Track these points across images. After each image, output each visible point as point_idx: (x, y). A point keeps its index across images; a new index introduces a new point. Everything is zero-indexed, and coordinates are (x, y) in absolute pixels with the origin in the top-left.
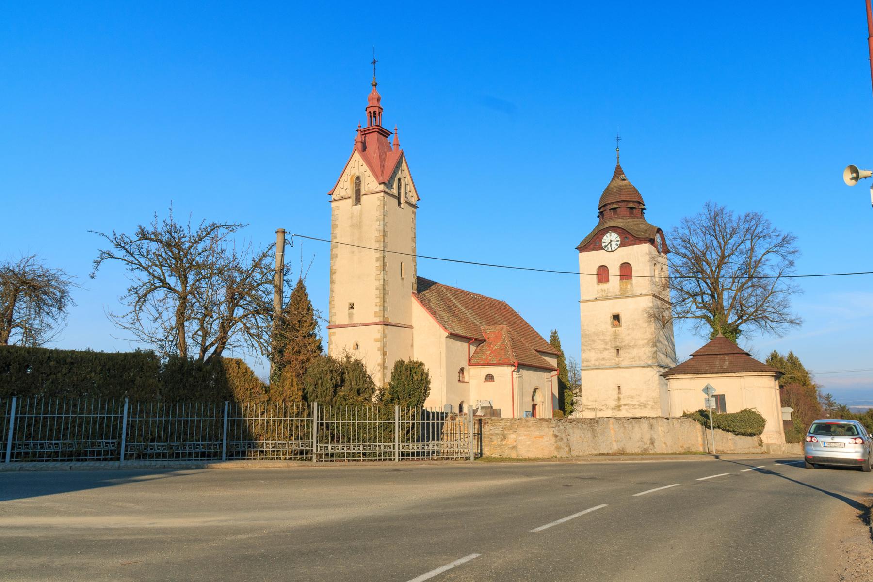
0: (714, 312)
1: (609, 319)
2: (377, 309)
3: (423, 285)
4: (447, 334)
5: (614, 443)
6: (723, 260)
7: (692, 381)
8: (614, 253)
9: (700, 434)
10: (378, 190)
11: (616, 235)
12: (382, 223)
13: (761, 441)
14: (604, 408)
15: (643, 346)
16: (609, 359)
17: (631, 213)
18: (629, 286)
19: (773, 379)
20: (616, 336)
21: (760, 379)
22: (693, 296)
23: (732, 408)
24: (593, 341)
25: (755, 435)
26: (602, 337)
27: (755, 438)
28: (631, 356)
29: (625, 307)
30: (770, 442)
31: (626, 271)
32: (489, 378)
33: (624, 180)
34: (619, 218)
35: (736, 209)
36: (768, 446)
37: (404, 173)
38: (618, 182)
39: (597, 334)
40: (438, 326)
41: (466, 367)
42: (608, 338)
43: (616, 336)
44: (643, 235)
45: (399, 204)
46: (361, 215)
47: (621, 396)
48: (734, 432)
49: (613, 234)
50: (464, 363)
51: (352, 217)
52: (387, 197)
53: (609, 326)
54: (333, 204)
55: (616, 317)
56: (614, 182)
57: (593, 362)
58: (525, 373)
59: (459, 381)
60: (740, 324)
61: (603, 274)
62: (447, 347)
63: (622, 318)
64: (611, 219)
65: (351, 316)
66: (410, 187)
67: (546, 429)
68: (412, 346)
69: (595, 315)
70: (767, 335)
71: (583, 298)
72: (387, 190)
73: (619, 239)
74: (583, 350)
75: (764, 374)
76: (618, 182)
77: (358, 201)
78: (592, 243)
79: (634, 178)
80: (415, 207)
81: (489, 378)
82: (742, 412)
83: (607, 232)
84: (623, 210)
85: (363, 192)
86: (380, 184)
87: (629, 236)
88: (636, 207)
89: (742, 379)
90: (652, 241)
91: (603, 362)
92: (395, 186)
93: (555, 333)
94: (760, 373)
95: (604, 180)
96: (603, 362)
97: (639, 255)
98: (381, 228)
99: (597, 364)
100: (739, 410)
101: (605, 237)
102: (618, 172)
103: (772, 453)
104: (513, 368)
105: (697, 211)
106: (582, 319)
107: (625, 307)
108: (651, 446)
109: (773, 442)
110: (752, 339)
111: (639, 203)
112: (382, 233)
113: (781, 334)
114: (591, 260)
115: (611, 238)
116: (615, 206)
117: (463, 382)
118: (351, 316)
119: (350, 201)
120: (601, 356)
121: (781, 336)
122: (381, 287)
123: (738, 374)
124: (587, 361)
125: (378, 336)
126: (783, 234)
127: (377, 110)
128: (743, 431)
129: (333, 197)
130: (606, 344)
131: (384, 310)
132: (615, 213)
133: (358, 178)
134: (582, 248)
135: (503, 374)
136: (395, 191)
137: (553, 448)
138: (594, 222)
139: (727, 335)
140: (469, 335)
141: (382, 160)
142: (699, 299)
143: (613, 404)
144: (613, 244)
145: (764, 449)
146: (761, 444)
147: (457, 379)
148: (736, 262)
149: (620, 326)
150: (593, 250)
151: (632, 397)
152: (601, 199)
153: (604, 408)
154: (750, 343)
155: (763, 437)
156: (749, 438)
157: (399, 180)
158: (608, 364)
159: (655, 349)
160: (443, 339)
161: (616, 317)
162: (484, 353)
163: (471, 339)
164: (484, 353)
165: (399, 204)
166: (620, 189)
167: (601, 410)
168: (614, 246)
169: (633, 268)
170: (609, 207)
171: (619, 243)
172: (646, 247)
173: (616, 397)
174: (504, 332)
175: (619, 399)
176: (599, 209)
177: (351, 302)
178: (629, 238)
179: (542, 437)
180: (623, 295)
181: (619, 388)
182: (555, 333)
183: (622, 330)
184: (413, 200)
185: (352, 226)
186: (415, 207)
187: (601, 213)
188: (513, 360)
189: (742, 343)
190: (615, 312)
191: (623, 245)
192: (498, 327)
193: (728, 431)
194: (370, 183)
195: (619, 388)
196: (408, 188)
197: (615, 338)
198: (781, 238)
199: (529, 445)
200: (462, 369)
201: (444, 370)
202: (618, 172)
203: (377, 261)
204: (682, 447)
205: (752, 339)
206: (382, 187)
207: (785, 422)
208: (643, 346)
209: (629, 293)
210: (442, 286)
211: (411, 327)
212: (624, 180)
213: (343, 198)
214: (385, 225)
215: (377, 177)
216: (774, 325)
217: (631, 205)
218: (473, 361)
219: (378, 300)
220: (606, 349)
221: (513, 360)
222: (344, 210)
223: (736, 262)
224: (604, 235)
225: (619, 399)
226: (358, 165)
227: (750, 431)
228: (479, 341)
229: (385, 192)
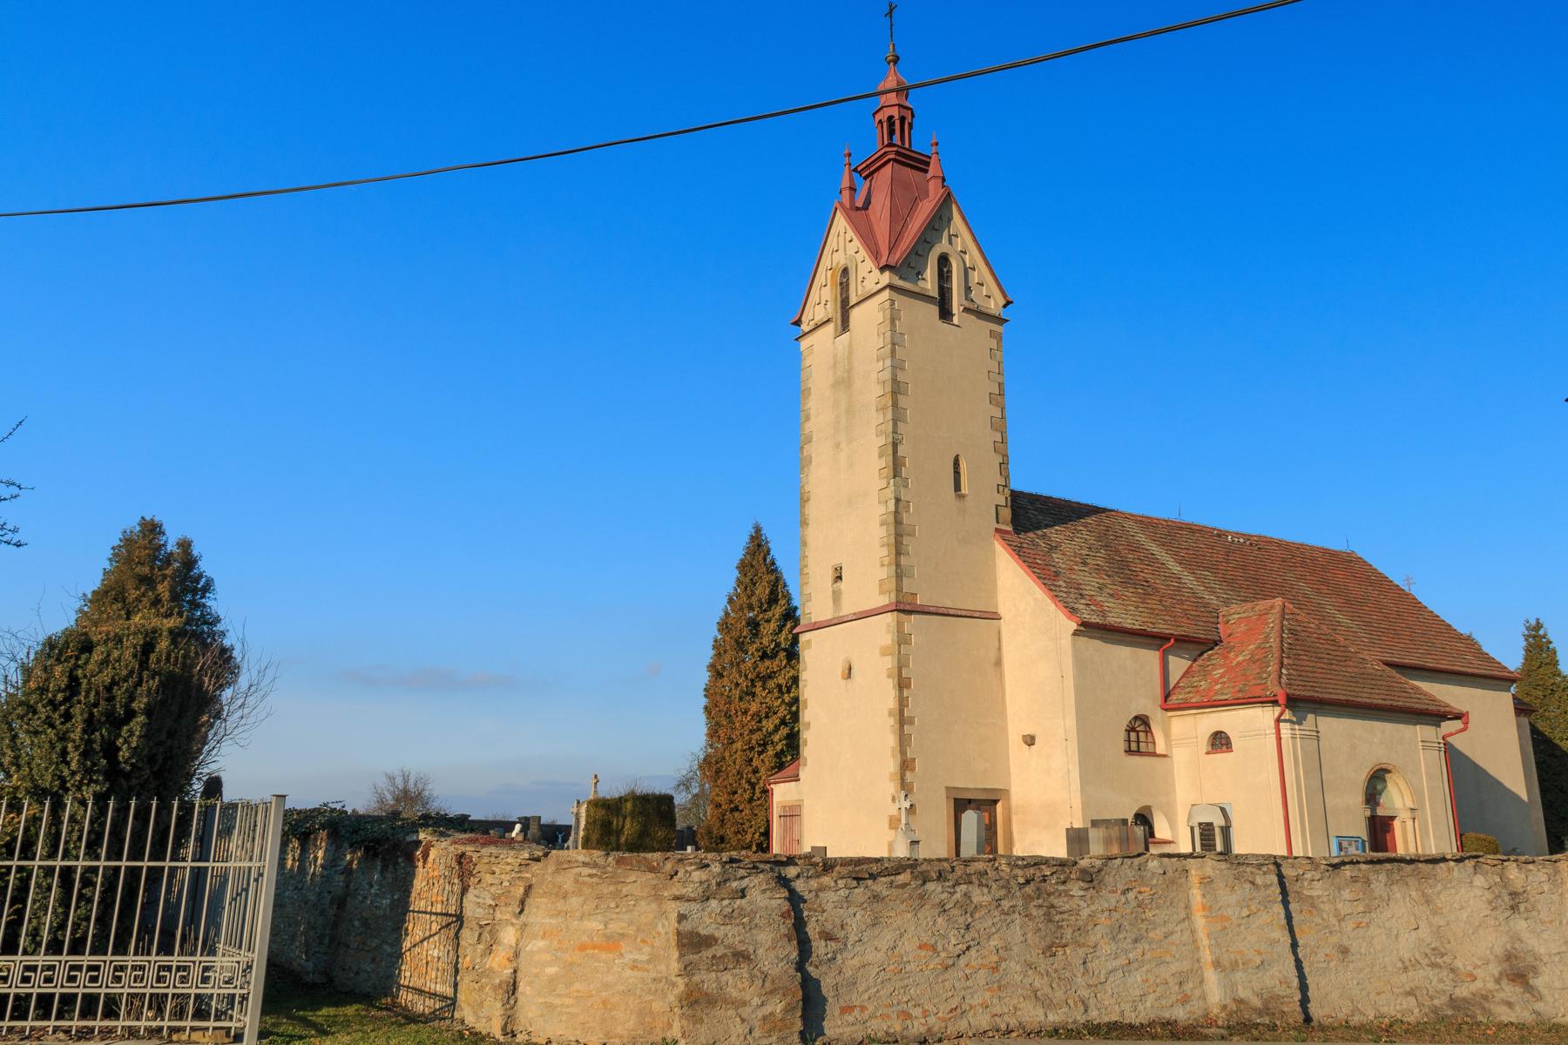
2: (883, 573)
3: (1031, 517)
4: (1074, 626)
5: (1211, 976)
10: (880, 286)
12: (888, 362)
32: (1220, 741)
37: (960, 241)
40: (1052, 607)
41: (1157, 717)
45: (946, 314)
46: (850, 353)
50: (1147, 703)
51: (835, 365)
52: (900, 300)
54: (804, 344)
58: (1331, 726)
59: (1129, 751)
62: (1080, 664)
65: (837, 597)
66: (981, 273)
67: (647, 910)
68: (998, 663)
72: (901, 283)
77: (845, 325)
80: (1000, 321)
81: (1220, 741)
85: (853, 300)
86: (882, 269)
92: (930, 273)
93: (1539, 626)
98: (887, 375)
104: (1278, 710)
108: (1510, 991)
112: (888, 389)
117: (1154, 754)
118: (837, 597)
119: (830, 327)
122: (891, 519)
125: (887, 639)
127: (895, 112)
129: (805, 327)
131: (900, 574)
133: (845, 271)
135: (1254, 725)
136: (929, 283)
137: (665, 1002)
140: (1162, 628)
141: (899, 219)
147: (1122, 746)
157: (944, 260)
160: (1067, 640)
162: (1206, 674)
163: (1164, 638)
164: (1205, 676)
165: (946, 314)
174: (1273, 619)
177: (836, 562)
179: (611, 943)
182: (1539, 626)
184: (994, 305)
185: (837, 384)
186: (1000, 321)
188: (1273, 688)
192: (1262, 605)
194: (869, 277)
196: (975, 277)
199: (552, 980)
200: (1140, 726)
201: (1071, 722)
203: (880, 457)
206: (886, 278)
210: (1128, 517)
211: (995, 617)
213: (817, 327)
214: (897, 367)
215: (875, 254)
218: (1174, 699)
219: (884, 552)
221: (1273, 688)
222: (820, 348)
226: (843, 245)
228: (1200, 645)
229: (890, 287)
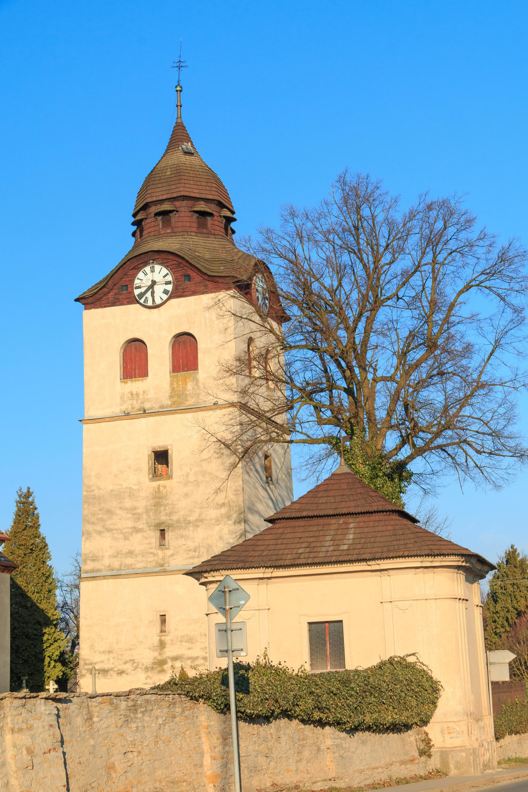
0: (351, 424)
1: (145, 460)
6: (372, 302)
7: (263, 586)
8: (160, 314)
9: (209, 745)
11: (165, 271)
13: (427, 741)
14: (128, 667)
15: (218, 521)
16: (143, 554)
17: (202, 226)
18: (190, 386)
19: (461, 576)
20: (159, 500)
21: (429, 575)
22: (308, 394)
23: (359, 656)
24: (110, 512)
25: (407, 727)
26: (128, 503)
27: (411, 737)
28: (192, 545)
29: (181, 434)
30: (450, 742)
31: (185, 350)
33: (188, 153)
34: (174, 233)
35: (402, 193)
36: (444, 754)
38: (178, 157)
39: (118, 495)
42: (141, 504)
43: (159, 500)
44: (221, 270)
47: (167, 639)
48: (338, 724)
49: (157, 267)
53: (144, 475)
55: (162, 457)
56: (168, 156)
57: (106, 562)
60: (411, 458)
61: (134, 357)
63: (174, 457)
64: (158, 236)
69: (114, 453)
70: (469, 485)
71: (90, 412)
73: (170, 278)
74: (88, 534)
75: (438, 561)
76: (178, 157)
78: (114, 290)
79: (213, 151)
82: (381, 666)
83: (146, 264)
84: (184, 216)
87: (193, 274)
88: (215, 212)
89: (385, 579)
90: (244, 288)
91: (129, 561)
94: (428, 562)
95: (150, 153)
96: (129, 561)
97: (216, 321)
99: (116, 564)
100: (374, 662)
101: (141, 275)
102: (179, 135)
103: (453, 772)
105: (319, 196)
106: (86, 462)
107: (181, 434)
109: (457, 742)
110: (436, 495)
111: (221, 205)
113: (500, 482)
114: (107, 328)
115: (155, 277)
116: (166, 207)
120: (124, 546)
121: (497, 487)
123: (374, 565)
124: (95, 559)
126: (501, 243)
128: (368, 719)
130: (138, 517)
132: (167, 224)
134: (93, 299)
138: (124, 244)
139: (379, 482)
142: (323, 398)
143: (148, 656)
144: (159, 290)
145: (434, 763)
146: (426, 750)
148: (399, 319)
149: (170, 477)
150: (113, 304)
151: (191, 640)
152: (141, 194)
153: (128, 667)
154: (430, 502)
155: (433, 730)
156: (393, 737)
158: (139, 564)
159: (242, 526)
161: (162, 457)
166: (179, 172)
167: (121, 673)
168: (159, 294)
169: (201, 346)
170: (154, 209)
171: (170, 288)
172: (229, 300)
173: (156, 640)
175: (162, 645)
176: (134, 215)
178: (191, 278)
180: (178, 406)
181: (163, 619)
182: (29, 494)
183: (174, 485)
187: (138, 223)
189: (412, 501)
190: (160, 444)
191: (178, 292)
193: (321, 723)
195: (163, 619)
197: (157, 505)
198: (494, 256)
202: (179, 135)
204: (350, 737)
205: (436, 495)
207: (496, 686)
208: (218, 521)
209: (191, 402)
212: (188, 153)
216: (483, 460)
217: (202, 207)
220: (136, 530)
223: (399, 319)
224: (138, 269)
225: (162, 645)
227: (389, 718)
